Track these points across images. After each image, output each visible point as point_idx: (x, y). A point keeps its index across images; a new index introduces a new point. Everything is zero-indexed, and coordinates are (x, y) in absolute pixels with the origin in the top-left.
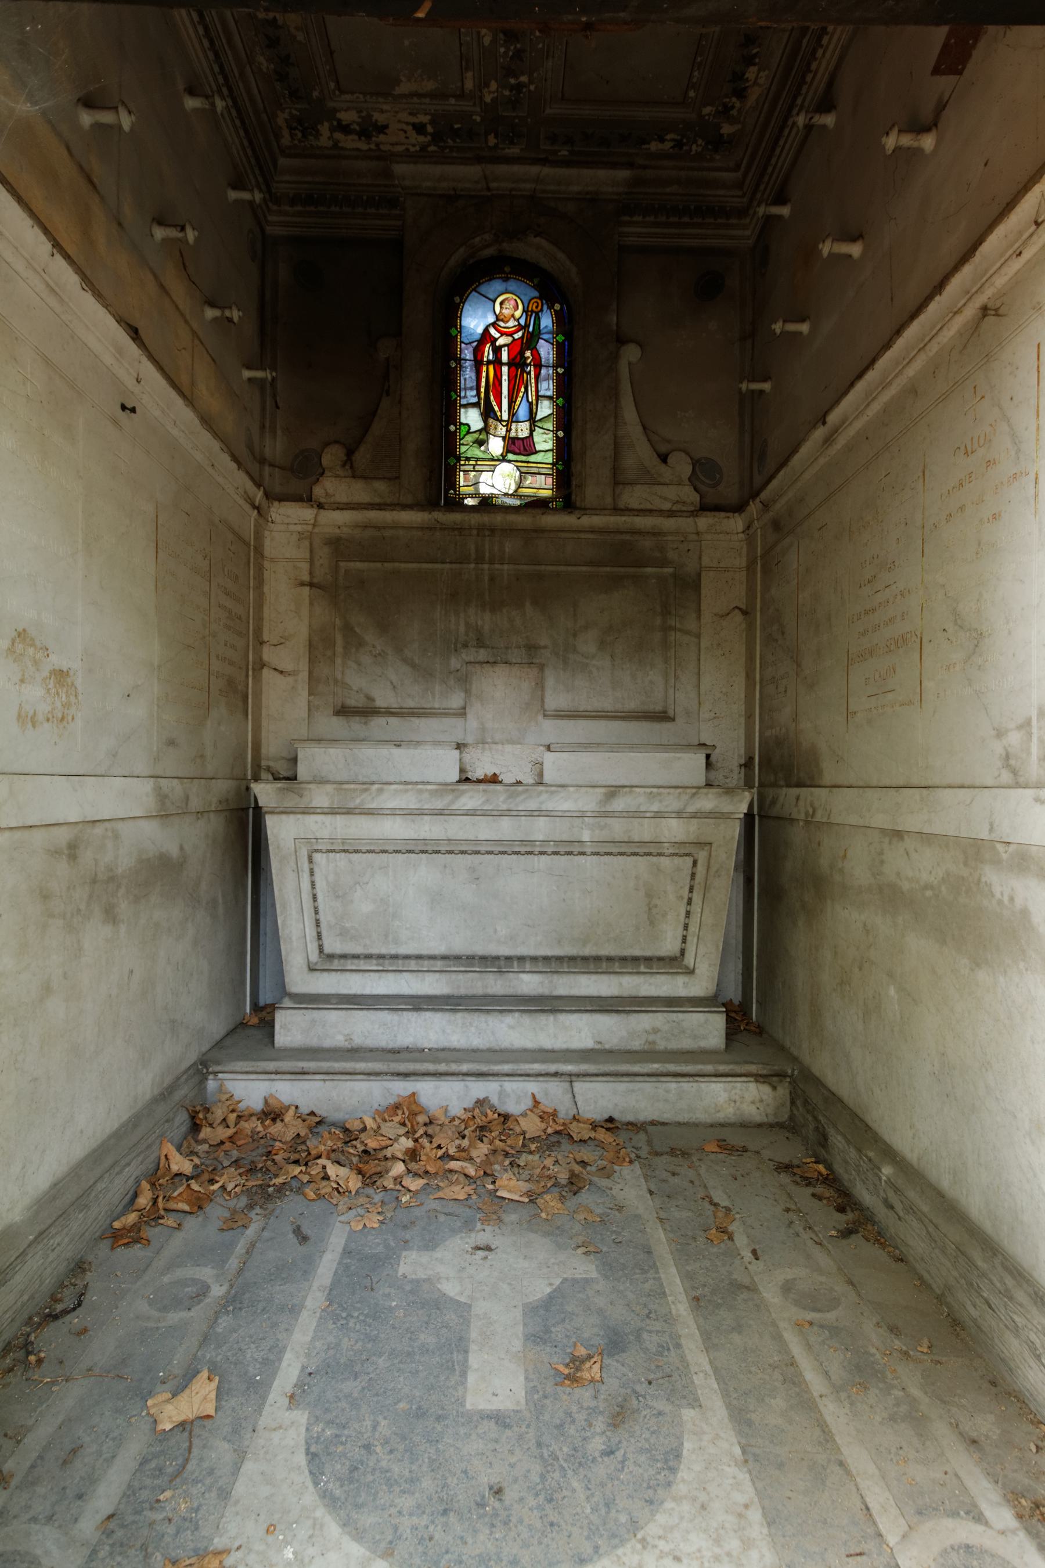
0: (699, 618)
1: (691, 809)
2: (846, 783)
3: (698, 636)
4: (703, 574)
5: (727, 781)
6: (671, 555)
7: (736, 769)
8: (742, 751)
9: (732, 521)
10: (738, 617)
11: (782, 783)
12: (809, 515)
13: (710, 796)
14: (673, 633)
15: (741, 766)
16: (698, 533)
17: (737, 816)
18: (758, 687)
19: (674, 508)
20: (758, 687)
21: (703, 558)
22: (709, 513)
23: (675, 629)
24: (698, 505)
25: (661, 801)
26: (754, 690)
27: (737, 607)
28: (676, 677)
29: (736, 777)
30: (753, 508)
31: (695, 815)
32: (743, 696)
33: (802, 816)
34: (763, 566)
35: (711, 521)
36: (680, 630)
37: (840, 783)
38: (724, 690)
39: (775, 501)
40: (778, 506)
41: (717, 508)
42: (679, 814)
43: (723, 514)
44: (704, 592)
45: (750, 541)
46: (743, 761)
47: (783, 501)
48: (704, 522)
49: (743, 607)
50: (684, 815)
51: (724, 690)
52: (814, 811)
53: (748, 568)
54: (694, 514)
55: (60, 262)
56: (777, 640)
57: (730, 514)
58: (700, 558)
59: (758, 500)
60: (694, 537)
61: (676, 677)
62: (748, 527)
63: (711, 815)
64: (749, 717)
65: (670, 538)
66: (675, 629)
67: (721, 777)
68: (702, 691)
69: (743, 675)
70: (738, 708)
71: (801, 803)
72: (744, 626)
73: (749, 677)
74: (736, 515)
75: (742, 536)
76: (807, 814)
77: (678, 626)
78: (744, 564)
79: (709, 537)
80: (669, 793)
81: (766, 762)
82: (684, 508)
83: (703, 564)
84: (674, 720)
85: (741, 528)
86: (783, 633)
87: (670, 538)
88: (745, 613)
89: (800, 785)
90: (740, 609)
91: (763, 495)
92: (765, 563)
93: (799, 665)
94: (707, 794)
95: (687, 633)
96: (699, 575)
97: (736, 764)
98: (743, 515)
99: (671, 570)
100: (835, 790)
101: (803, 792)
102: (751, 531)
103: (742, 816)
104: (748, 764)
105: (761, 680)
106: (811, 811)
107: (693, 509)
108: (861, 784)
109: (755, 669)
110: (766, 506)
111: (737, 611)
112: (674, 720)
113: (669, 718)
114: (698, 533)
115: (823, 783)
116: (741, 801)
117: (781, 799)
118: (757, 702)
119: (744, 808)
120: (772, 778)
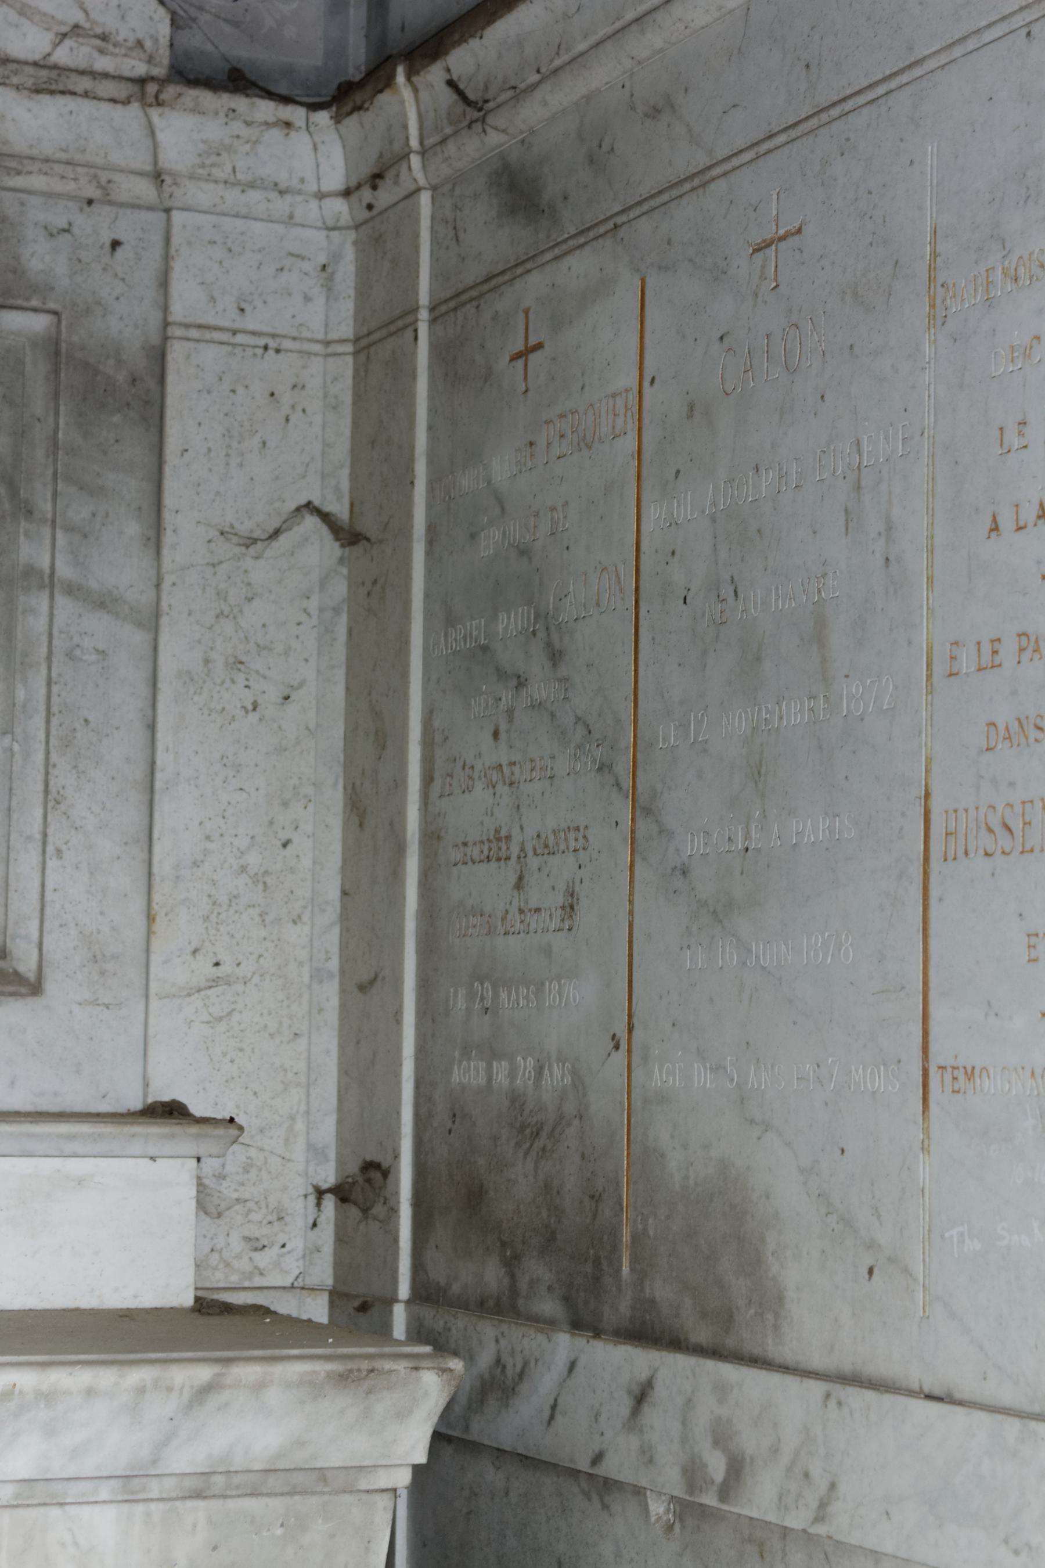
0: (155, 538)
1: (187, 1458)
2: (915, 1375)
3: (152, 621)
4: (176, 353)
5: (263, 1259)
6: (40, 258)
7: (301, 1209)
8: (327, 1131)
9: (301, 141)
10: (317, 548)
11: (549, 1306)
12: (699, 179)
13: (273, 1396)
14: (41, 601)
15: (320, 1193)
16: (158, 177)
17: (384, 1480)
18: (412, 865)
19: (62, 56)
20: (412, 865)
21: (177, 286)
22: (206, 98)
23: (49, 582)
24: (164, 56)
25: (50, 1431)
26: (397, 874)
27: (309, 507)
28: (51, 798)
29: (297, 1244)
30: (410, 103)
31: (200, 1488)
32: (333, 892)
33: (670, 1478)
34: (441, 353)
35: (214, 130)
36: (72, 590)
37: (880, 1368)
38: (253, 860)
39: (519, 93)
40: (531, 113)
41: (237, 80)
42: (131, 1485)
43: (266, 109)
44: (177, 431)
45: (379, 237)
46: (328, 1177)
47: (560, 96)
48: (188, 129)
49: (340, 509)
50: (154, 1489)
51: (253, 860)
52: (736, 1468)
53: (364, 345)
54: (144, 91)
55: (229, 1501)
56: (521, 682)
57: (297, 114)
58: (164, 283)
59: (434, 75)
60: (145, 189)
61: (51, 798)
62: (376, 179)
63: (274, 1482)
64: (365, 986)
65: (38, 182)
66: (49, 582)
67: (236, 1244)
68: (163, 865)
69: (335, 797)
70: (313, 938)
71: (660, 1419)
72: (340, 588)
73: (367, 808)
74: (323, 117)
75: (339, 207)
76: (693, 1473)
77: (65, 570)
78: (346, 329)
79: (202, 194)
80: (90, 1392)
81: (457, 1197)
82: (103, 64)
83: (177, 312)
84: (35, 988)
85: (335, 178)
86: (555, 656)
87: (38, 182)
88: (348, 535)
89: (646, 1332)
90: (325, 517)
91: (463, 59)
92: (456, 331)
93: (643, 808)
94: (259, 1387)
95: (104, 602)
96: (159, 357)
97: (299, 1186)
98: (352, 122)
99: (39, 323)
100: (856, 1398)
101: (673, 1369)
102: (384, 197)
103: (403, 1478)
104: (358, 1190)
105: (431, 837)
106: (717, 1466)
107: (141, 69)
108: (1007, 1396)
109: (399, 784)
110: (472, 106)
111: (311, 521)
112: (35, 988)
113: (18, 978)
114: (158, 177)
115: (787, 1352)
116: (402, 1415)
117: (544, 1384)
118: (410, 926)
119: (414, 1444)
120: (492, 1275)
